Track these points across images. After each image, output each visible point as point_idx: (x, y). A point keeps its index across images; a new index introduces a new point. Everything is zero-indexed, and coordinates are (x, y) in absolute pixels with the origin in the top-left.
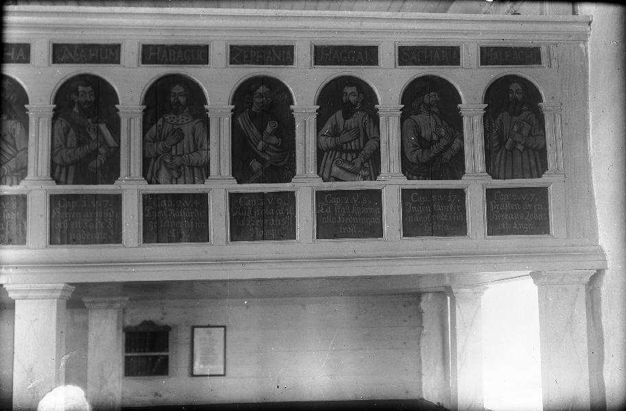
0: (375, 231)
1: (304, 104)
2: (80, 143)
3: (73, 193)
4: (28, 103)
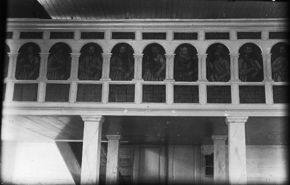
0: (263, 101)
1: (76, 54)
2: (248, 67)
3: (247, 85)
4: (134, 53)
